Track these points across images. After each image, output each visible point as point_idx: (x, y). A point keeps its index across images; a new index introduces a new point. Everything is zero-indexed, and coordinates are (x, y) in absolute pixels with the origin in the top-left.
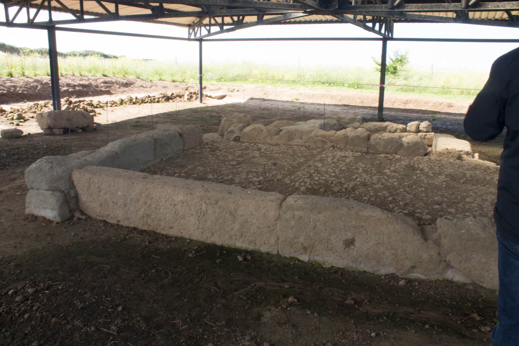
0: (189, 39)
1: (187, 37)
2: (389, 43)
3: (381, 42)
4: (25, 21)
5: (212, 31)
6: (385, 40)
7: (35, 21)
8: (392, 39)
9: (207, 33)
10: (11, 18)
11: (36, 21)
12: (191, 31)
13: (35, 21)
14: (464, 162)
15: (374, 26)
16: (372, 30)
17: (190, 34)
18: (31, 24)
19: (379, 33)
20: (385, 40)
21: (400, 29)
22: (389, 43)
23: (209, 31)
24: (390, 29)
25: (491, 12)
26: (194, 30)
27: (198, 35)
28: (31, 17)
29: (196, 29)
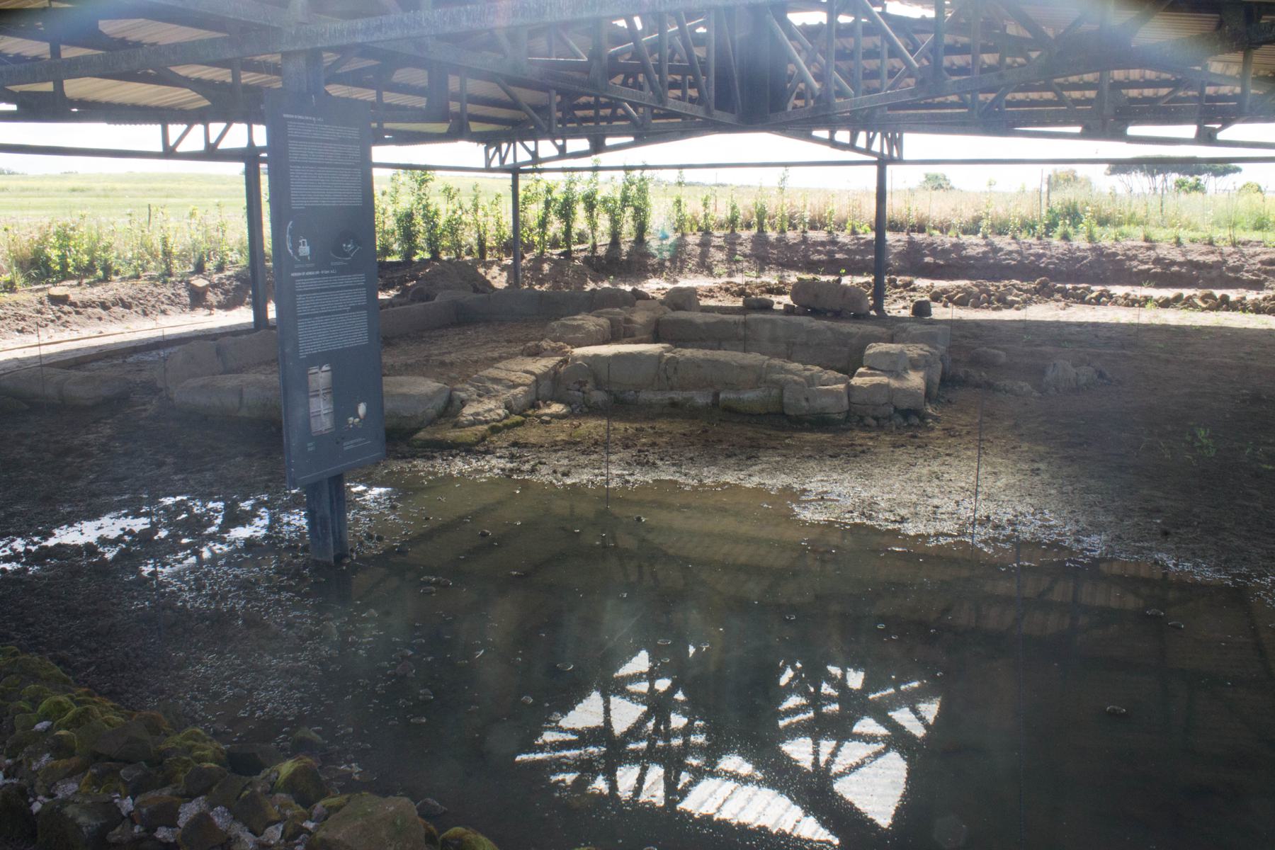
0: (488, 169)
1: (483, 165)
2: (890, 169)
3: (874, 169)
4: (200, 146)
5: (569, 150)
6: (882, 163)
7: (220, 147)
8: (900, 161)
9: (556, 152)
10: (171, 143)
11: (222, 146)
12: (492, 151)
13: (220, 147)
14: (450, 425)
15: (854, 137)
16: (851, 147)
17: (488, 160)
18: (211, 153)
19: (867, 151)
20: (882, 163)
21: (916, 144)
22: (890, 169)
23: (562, 149)
24: (896, 143)
25: (791, 169)
26: (499, 149)
27: (509, 161)
28: (212, 141)
29: (504, 146)
